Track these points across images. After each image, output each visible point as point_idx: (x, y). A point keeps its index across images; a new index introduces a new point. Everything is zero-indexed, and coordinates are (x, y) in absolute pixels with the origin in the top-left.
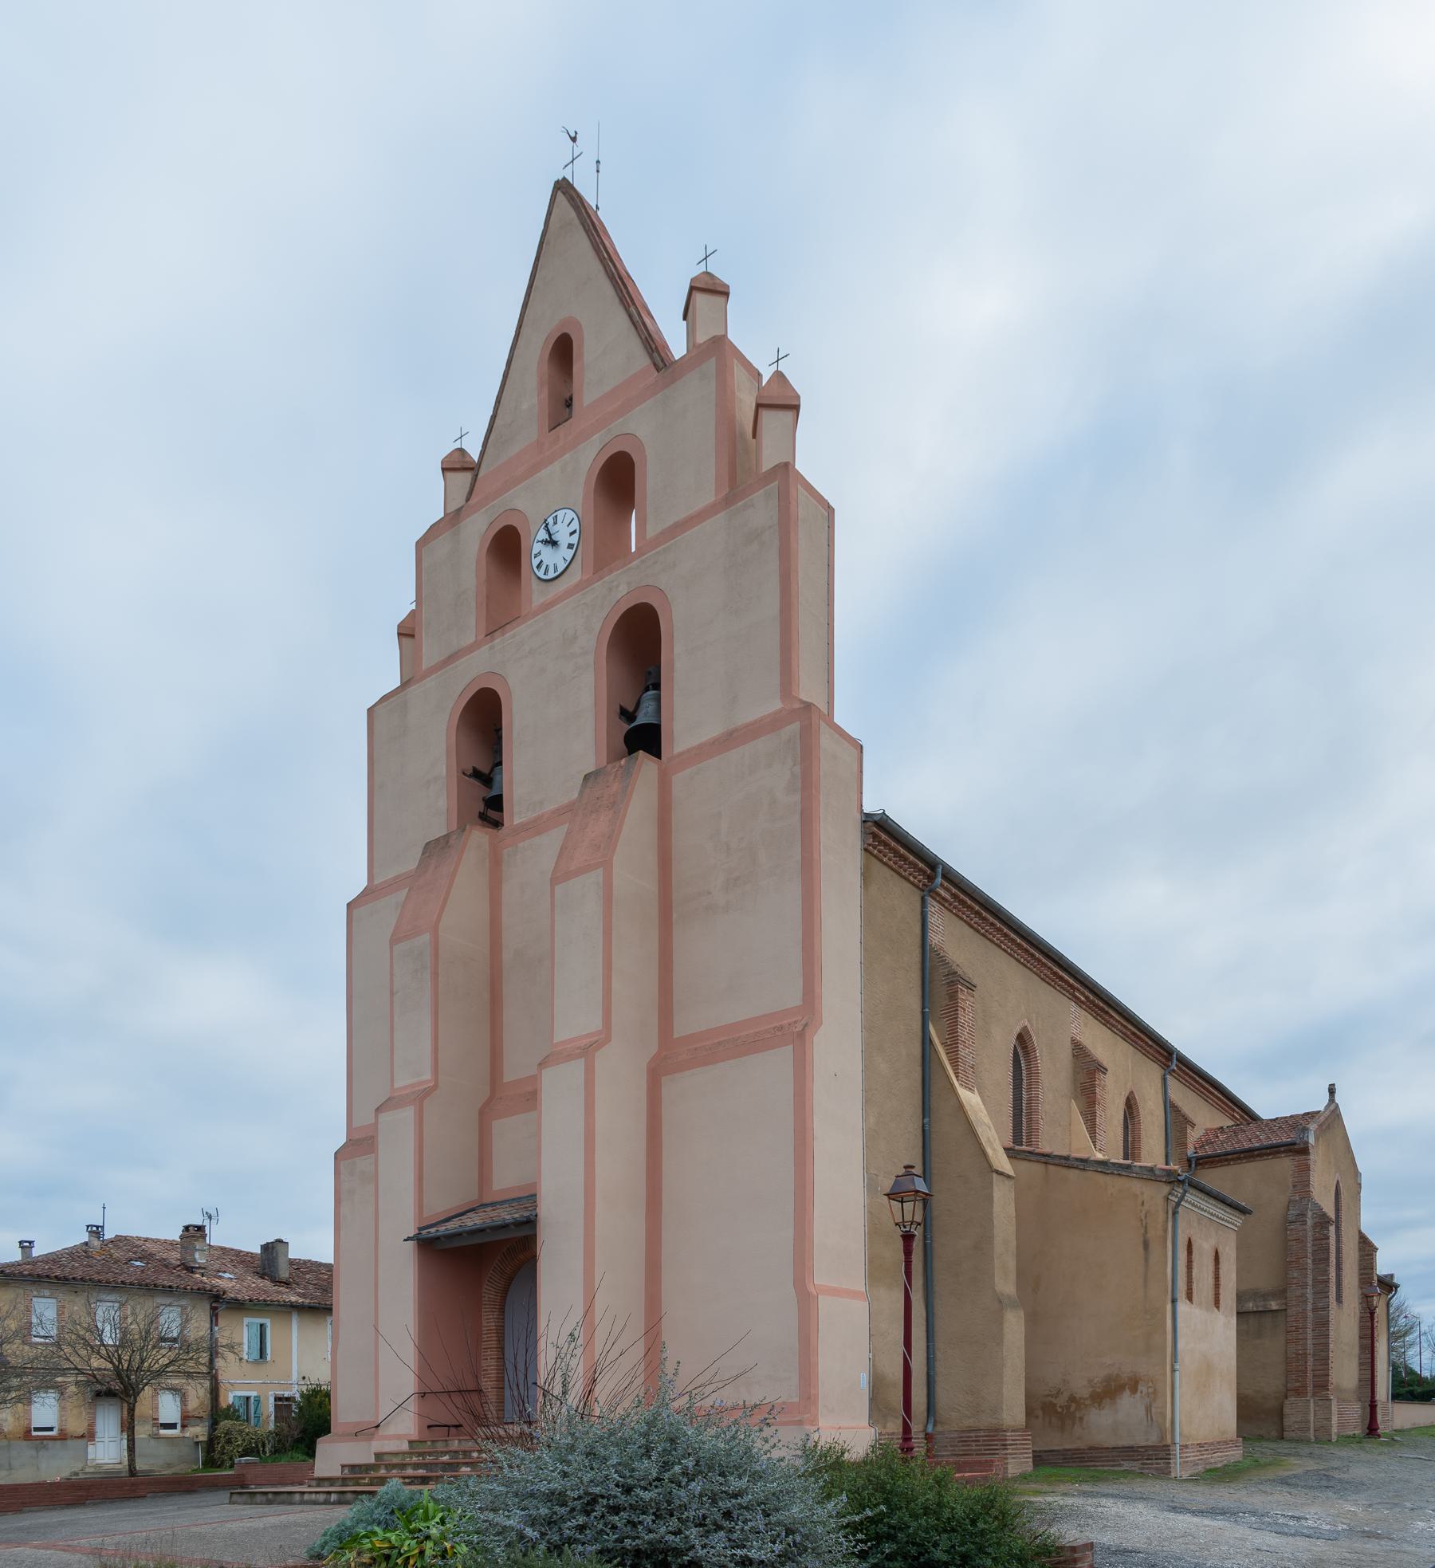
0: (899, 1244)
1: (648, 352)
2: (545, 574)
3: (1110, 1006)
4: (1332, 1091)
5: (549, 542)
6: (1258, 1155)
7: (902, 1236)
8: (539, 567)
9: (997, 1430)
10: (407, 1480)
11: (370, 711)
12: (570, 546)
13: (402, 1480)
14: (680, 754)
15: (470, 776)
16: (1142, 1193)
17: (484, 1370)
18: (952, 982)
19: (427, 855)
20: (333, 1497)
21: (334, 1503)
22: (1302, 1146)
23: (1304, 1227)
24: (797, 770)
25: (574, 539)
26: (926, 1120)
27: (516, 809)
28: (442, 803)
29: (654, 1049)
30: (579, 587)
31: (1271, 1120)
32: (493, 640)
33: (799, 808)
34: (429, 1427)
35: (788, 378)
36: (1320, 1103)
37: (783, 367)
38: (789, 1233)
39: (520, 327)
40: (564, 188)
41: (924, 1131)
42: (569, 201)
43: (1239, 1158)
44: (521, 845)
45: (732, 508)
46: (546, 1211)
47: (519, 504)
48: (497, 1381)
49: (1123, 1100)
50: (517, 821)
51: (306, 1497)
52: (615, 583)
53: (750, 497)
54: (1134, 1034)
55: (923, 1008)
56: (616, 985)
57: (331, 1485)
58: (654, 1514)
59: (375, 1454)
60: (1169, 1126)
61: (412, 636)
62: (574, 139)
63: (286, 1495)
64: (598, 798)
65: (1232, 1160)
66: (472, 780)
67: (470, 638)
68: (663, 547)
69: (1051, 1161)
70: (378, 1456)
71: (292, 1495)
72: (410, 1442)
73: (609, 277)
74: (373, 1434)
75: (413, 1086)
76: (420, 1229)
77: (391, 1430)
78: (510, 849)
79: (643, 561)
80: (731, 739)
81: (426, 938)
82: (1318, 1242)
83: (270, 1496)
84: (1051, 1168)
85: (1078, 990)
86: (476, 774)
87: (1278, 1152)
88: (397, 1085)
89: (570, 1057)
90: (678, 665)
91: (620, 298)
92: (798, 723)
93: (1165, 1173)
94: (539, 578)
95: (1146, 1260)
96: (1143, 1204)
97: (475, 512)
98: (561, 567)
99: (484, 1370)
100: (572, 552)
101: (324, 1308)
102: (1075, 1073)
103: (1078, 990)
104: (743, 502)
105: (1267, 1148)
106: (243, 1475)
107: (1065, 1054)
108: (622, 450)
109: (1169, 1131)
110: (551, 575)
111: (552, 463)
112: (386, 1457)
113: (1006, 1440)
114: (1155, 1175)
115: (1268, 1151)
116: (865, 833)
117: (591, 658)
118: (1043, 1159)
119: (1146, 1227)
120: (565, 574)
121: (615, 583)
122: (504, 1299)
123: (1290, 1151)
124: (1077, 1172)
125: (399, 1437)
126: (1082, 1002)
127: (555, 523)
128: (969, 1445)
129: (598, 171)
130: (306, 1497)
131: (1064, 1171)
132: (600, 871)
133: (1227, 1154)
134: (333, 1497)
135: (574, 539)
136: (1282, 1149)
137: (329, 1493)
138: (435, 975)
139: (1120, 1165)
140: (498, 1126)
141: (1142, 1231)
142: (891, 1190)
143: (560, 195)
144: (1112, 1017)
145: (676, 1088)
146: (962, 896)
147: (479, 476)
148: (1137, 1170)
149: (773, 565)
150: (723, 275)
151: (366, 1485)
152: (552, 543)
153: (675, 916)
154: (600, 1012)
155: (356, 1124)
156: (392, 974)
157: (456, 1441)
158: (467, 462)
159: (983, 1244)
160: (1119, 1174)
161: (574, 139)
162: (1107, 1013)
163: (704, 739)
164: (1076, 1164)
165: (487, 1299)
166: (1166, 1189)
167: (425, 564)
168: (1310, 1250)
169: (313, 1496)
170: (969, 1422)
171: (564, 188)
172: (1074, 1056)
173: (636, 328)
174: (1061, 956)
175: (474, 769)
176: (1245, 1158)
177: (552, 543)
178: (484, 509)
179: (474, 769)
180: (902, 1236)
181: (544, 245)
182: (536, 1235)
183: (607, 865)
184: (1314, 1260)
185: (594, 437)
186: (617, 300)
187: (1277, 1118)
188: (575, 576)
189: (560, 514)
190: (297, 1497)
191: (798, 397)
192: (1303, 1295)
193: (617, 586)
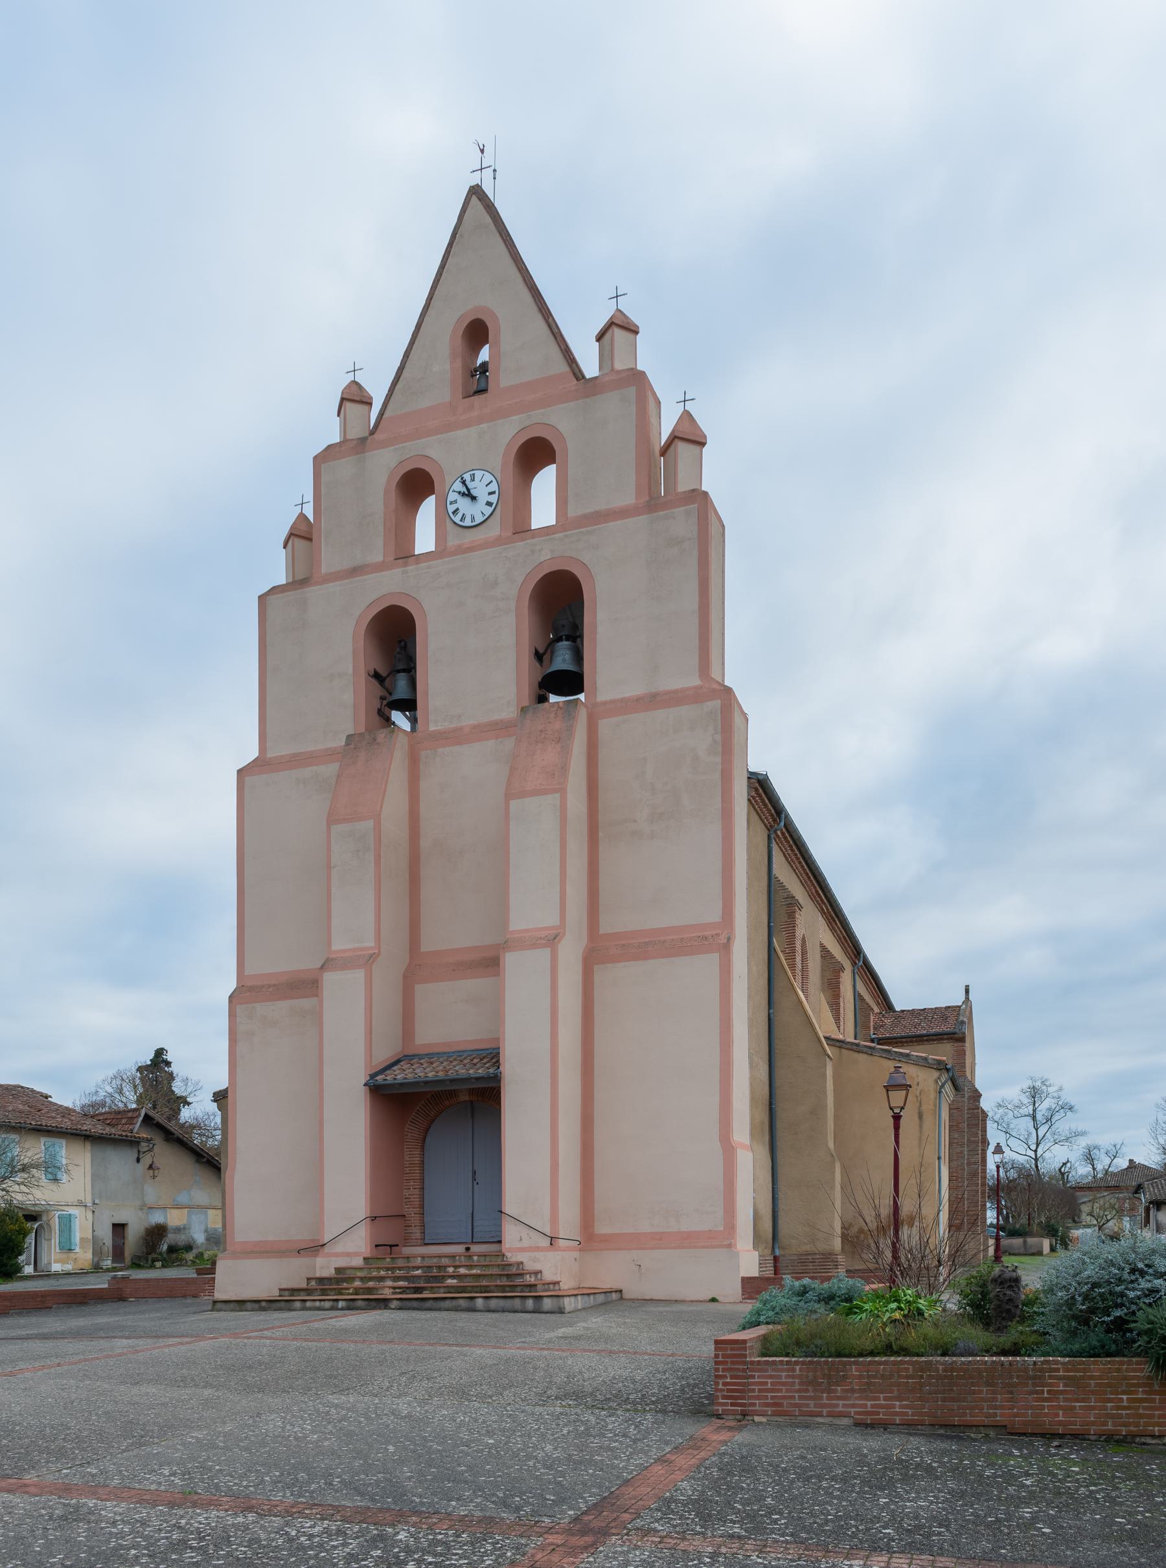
0: (891, 1122)
1: (568, 361)
2: (461, 521)
3: (837, 916)
4: (967, 991)
5: (467, 495)
6: (927, 1040)
7: (892, 1116)
9: (830, 1254)
10: (398, 1290)
11: (262, 599)
12: (489, 504)
13: (391, 1290)
14: (605, 703)
15: (372, 677)
16: (918, 1076)
17: (406, 1198)
18: (790, 904)
19: (352, 746)
20: (341, 1304)
21: (342, 1309)
22: (961, 1035)
23: (963, 1099)
24: (718, 737)
25: (493, 499)
26: (771, 1011)
27: (432, 717)
28: (348, 697)
29: (585, 942)
30: (498, 541)
31: (920, 1010)
32: (406, 565)
33: (719, 767)
34: (376, 1246)
35: (696, 419)
36: (957, 1000)
37: (689, 406)
38: (716, 1099)
39: (431, 299)
40: (476, 192)
41: (769, 1019)
42: (486, 209)
43: (912, 1042)
44: (440, 750)
45: (654, 514)
46: (509, 1069)
47: (433, 454)
48: (419, 1208)
50: (432, 728)
51: (308, 1304)
52: (538, 547)
53: (672, 510)
54: (844, 937)
55: (769, 923)
56: (569, 889)
57: (308, 1295)
59: (335, 1269)
60: (857, 1011)
61: (310, 540)
62: (482, 151)
63: (431, 1301)
64: (541, 731)
65: (906, 1042)
66: (373, 680)
67: (377, 557)
68: (586, 529)
69: (845, 1046)
70: (338, 1270)
71: (292, 1303)
72: (766, 1248)
73: (528, 287)
74: (318, 1251)
75: (355, 950)
76: (372, 1076)
77: (339, 1248)
78: (429, 751)
79: (566, 536)
80: (653, 701)
81: (370, 823)
82: (971, 1111)
83: (264, 1304)
84: (844, 1051)
86: (376, 676)
87: (942, 1039)
88: (334, 948)
89: (534, 946)
90: (600, 629)
91: (538, 307)
92: (719, 701)
93: (935, 1062)
94: (455, 523)
95: (921, 1126)
96: (918, 1084)
97: (382, 448)
99: (406, 1198)
100: (491, 509)
101: (58, 1132)
102: (823, 970)
104: (665, 512)
105: (945, 1034)
106: (121, 1289)
107: (818, 950)
108: (548, 438)
109: (857, 1015)
110: (468, 522)
111: (469, 427)
112: (348, 1272)
113: (837, 1262)
114: (928, 1063)
115: (935, 1037)
116: (750, 786)
117: (513, 605)
118: (838, 1044)
119: (920, 1102)
120: (485, 524)
121: (538, 547)
122: (424, 1139)
123: (951, 1039)
124: (865, 1056)
125: (356, 1254)
126: (825, 913)
128: (806, 1266)
129: (495, 178)
130: (308, 1304)
131: (856, 1055)
132: (558, 795)
133: (902, 1037)
134: (341, 1304)
135: (493, 499)
136: (945, 1037)
137: (337, 1300)
138: (378, 858)
139: (852, 1044)
140: (419, 989)
141: (918, 1105)
142: (888, 1082)
143: (474, 199)
144: (836, 924)
145: (604, 975)
146: (787, 834)
147: (384, 416)
148: (914, 1058)
149: (693, 571)
150: (635, 318)
151: (349, 1294)
152: (469, 495)
153: (601, 834)
154: (558, 911)
155: (248, 971)
156: (329, 850)
157: (419, 1259)
158: (365, 397)
160: (900, 1061)
161: (482, 151)
162: (834, 921)
163: (627, 695)
164: (865, 1050)
165: (409, 1137)
166: (936, 1074)
167: (324, 478)
168: (966, 1116)
169: (317, 1304)
170: (808, 1248)
171: (476, 192)
172: (822, 956)
173: (556, 338)
174: (824, 879)
175: (375, 671)
176: (916, 1041)
177: (469, 495)
178: (393, 447)
179: (375, 671)
180: (892, 1116)
181: (457, 236)
182: (500, 1087)
183: (562, 791)
184: (968, 1125)
185: (513, 418)
186: (535, 308)
187: (925, 1009)
188: (494, 530)
189: (478, 474)
190: (298, 1305)
191: (705, 437)
192: (962, 1152)
193: (540, 550)
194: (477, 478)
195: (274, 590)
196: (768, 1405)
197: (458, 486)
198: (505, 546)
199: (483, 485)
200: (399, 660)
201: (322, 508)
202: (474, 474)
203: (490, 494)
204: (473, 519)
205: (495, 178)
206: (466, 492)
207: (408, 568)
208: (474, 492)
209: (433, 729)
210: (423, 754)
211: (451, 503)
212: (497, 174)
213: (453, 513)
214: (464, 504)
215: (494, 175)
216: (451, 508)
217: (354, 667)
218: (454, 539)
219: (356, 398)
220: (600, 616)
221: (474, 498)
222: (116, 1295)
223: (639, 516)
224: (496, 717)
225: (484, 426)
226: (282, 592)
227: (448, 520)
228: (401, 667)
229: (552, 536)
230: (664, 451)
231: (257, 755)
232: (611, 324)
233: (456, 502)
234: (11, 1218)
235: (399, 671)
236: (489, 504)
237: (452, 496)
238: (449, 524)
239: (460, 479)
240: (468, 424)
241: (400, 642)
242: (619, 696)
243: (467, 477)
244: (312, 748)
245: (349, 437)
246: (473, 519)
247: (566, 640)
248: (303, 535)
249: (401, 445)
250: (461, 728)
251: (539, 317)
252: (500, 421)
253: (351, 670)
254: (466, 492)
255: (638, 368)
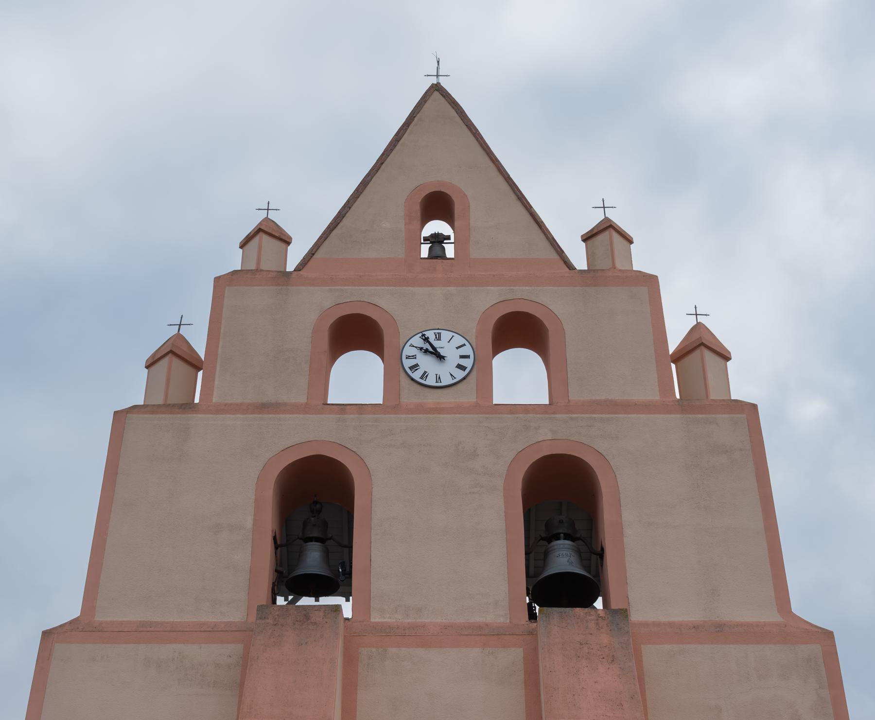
14: (646, 625)
28: (243, 557)
44: (393, 650)
45: (690, 416)
47: (382, 303)
78: (374, 650)
79: (572, 419)
94: (412, 379)
135: (468, 363)
150: (288, 228)
181: (416, 119)
195: (135, 408)
197: (417, 341)
198: (487, 416)
200: (314, 525)
201: (222, 331)
203: (462, 357)
206: (431, 349)
207: (346, 416)
208: (442, 352)
209: (377, 620)
210: (364, 651)
211: (408, 357)
214: (426, 363)
216: (408, 363)
217: (255, 521)
218: (409, 395)
219: (274, 233)
220: (627, 516)
221: (441, 358)
223: (670, 413)
224: (477, 618)
225: (452, 289)
226: (153, 412)
227: (403, 374)
228: (315, 534)
229: (553, 416)
230: (679, 357)
231: (79, 615)
232: (258, 231)
233: (414, 357)
235: (310, 539)
237: (408, 351)
238: (404, 381)
239: (420, 335)
240: (432, 283)
241: (315, 503)
242: (664, 619)
243: (431, 335)
244: (173, 617)
245: (264, 266)
247: (565, 539)
248: (183, 356)
249: (339, 287)
250: (424, 626)
251: (519, 204)
252: (474, 288)
253: (249, 523)
254: (431, 349)
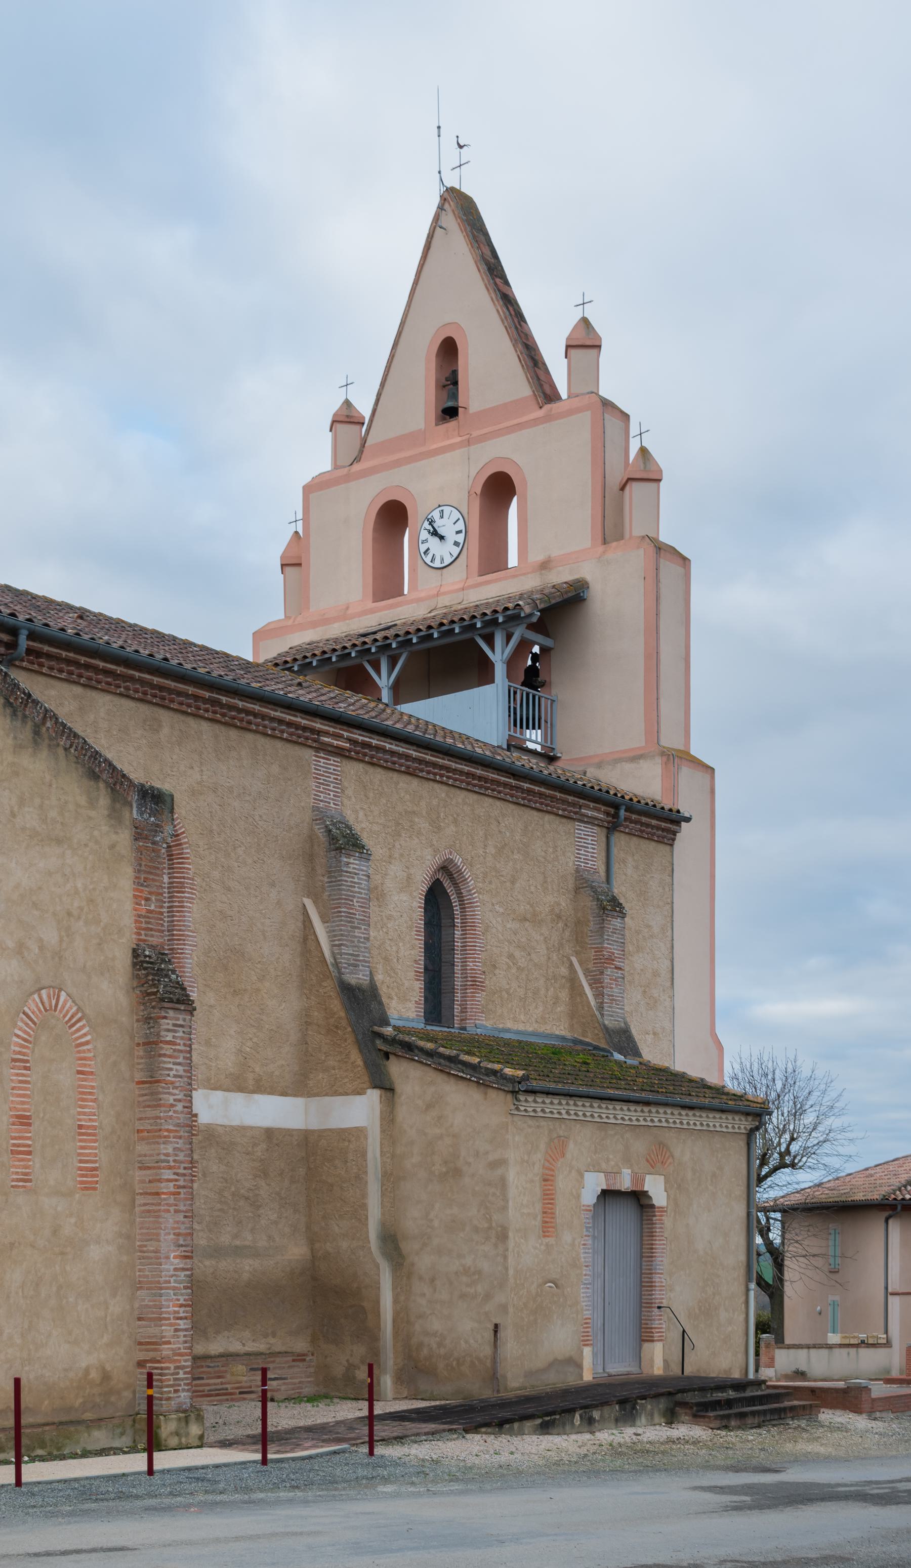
8: (426, 552)
12: (456, 544)
49: (421, 887)
58: (325, 1053)
85: (327, 733)
94: (425, 563)
98: (448, 560)
100: (463, 535)
103: (327, 733)
110: (437, 564)
127: (442, 517)
129: (439, 136)
135: (460, 538)
159: (74, 658)
189: (447, 510)
194: (446, 515)
196: (361, 971)
199: (449, 525)
202: (442, 511)
204: (442, 560)
205: (439, 136)
208: (441, 531)
212: (442, 130)
213: (425, 553)
214: (434, 542)
215: (439, 132)
216: (423, 548)
221: (442, 538)
222: (347, 478)
234: (359, 989)
236: (456, 544)
238: (420, 562)
243: (436, 514)
246: (442, 560)
255: (661, 539)
